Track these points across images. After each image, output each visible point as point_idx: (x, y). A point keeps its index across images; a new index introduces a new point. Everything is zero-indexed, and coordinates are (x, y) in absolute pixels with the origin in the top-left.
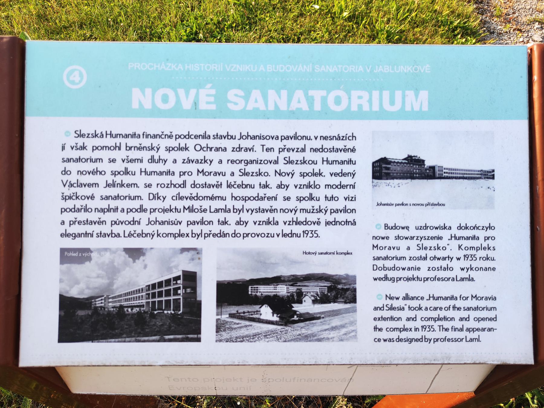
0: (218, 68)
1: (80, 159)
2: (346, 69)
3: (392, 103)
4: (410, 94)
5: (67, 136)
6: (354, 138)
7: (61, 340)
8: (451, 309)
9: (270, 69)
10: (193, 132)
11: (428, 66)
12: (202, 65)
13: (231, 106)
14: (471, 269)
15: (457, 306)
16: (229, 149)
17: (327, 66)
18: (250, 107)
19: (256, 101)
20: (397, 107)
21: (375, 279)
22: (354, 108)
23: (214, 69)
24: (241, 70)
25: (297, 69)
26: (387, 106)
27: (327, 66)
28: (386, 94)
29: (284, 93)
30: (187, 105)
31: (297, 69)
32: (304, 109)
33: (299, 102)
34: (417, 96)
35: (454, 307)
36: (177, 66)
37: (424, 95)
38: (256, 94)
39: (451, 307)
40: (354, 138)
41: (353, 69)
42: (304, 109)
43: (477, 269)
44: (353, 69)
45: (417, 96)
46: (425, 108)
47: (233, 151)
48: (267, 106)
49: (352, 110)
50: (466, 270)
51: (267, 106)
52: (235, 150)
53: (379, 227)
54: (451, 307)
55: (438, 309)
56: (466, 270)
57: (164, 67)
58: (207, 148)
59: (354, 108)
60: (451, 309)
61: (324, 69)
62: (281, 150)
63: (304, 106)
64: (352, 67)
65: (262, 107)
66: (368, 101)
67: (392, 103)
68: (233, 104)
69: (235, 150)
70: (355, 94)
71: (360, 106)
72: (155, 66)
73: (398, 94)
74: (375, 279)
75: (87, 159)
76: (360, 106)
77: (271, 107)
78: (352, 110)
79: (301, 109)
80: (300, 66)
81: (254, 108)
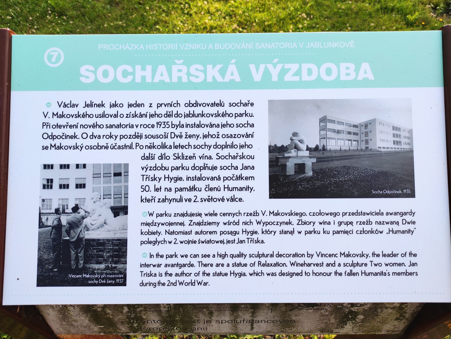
1: (120, 125)
5: (48, 106)
6: (178, 105)
7: (38, 285)
8: (408, 255)
9: (217, 47)
11: (352, 41)
12: (160, 45)
13: (83, 80)
17: (266, 44)
18: (360, 78)
19: (365, 72)
22: (210, 79)
23: (170, 48)
27: (266, 44)
29: (149, 68)
30: (257, 77)
32: (370, 79)
33: (232, 74)
36: (139, 46)
38: (162, 68)
39: (408, 254)
40: (178, 105)
41: (288, 45)
42: (370, 79)
44: (288, 45)
48: (171, 79)
49: (136, 81)
51: (171, 79)
54: (408, 254)
55: (220, 265)
57: (128, 47)
59: (210, 79)
61: (264, 46)
63: (237, 78)
64: (287, 44)
65: (167, 80)
66: (354, 71)
68: (194, 77)
70: (343, 66)
71: (180, 78)
72: (121, 47)
75: (127, 125)
76: (180, 78)
77: (175, 80)
78: (136, 81)
79: (164, 81)
80: (243, 44)
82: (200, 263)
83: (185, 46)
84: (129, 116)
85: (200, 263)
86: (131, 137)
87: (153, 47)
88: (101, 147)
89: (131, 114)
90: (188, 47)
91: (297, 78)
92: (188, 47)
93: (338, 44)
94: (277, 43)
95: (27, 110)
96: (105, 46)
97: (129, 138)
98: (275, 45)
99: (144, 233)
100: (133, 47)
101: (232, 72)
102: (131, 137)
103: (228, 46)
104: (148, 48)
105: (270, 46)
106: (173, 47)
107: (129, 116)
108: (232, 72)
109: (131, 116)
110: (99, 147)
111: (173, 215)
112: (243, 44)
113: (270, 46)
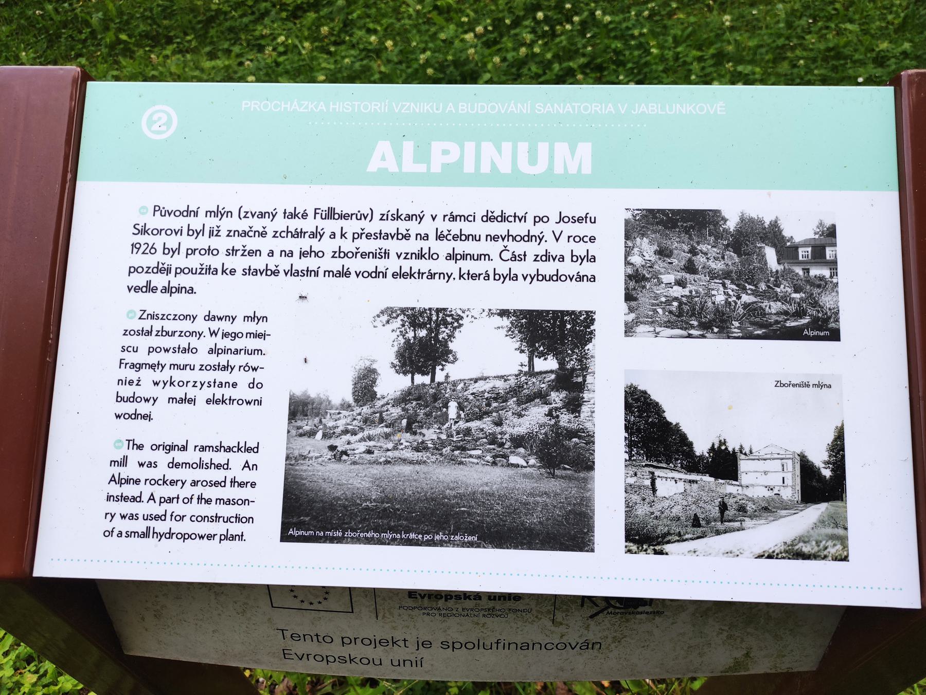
0: (380, 108)
2: (586, 108)
3: (533, 161)
4: (562, 148)
5: (143, 214)
8: (195, 500)
9: (462, 110)
10: (404, 212)
14: (172, 383)
15: (205, 496)
16: (530, 257)
19: (383, 159)
20: (541, 167)
21: (118, 416)
24: (418, 111)
25: (507, 109)
26: (524, 167)
28: (523, 147)
31: (507, 109)
33: (383, 159)
34: (573, 151)
35: (200, 499)
37: (585, 150)
39: (195, 498)
43: (181, 384)
45: (573, 151)
46: (587, 169)
47: (535, 260)
48: (400, 164)
50: (161, 384)
51: (400, 164)
52: (539, 258)
53: (130, 315)
54: (195, 498)
56: (161, 384)
58: (288, 232)
60: (195, 500)
62: (356, 236)
65: (393, 168)
67: (533, 161)
69: (539, 258)
73: (543, 148)
74: (118, 416)
80: (512, 105)
81: (379, 169)
82: (131, 443)
83: (403, 106)
84: (385, 217)
85: (131, 443)
86: (150, 271)
87: (343, 107)
88: (467, 238)
89: (390, 214)
90: (409, 108)
91: (421, 168)
92: (409, 108)
93: (694, 108)
94: (576, 104)
95: (105, 220)
96: (255, 104)
97: (147, 272)
98: (573, 108)
99: (175, 383)
100: (307, 107)
101: (383, 155)
102: (150, 271)
103: (482, 108)
104: (333, 109)
105: (564, 108)
106: (380, 108)
107: (385, 217)
108: (383, 155)
109: (390, 217)
110: (463, 237)
111: (198, 367)
112: (512, 105)
113: (564, 108)
